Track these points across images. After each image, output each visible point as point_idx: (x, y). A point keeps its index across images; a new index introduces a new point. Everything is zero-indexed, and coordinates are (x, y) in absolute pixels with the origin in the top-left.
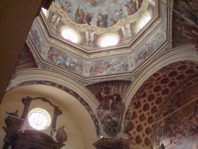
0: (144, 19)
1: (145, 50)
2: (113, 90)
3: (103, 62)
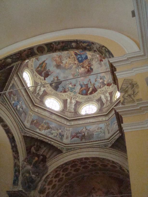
0: (89, 105)
1: (84, 132)
2: (43, 151)
3: (44, 121)
